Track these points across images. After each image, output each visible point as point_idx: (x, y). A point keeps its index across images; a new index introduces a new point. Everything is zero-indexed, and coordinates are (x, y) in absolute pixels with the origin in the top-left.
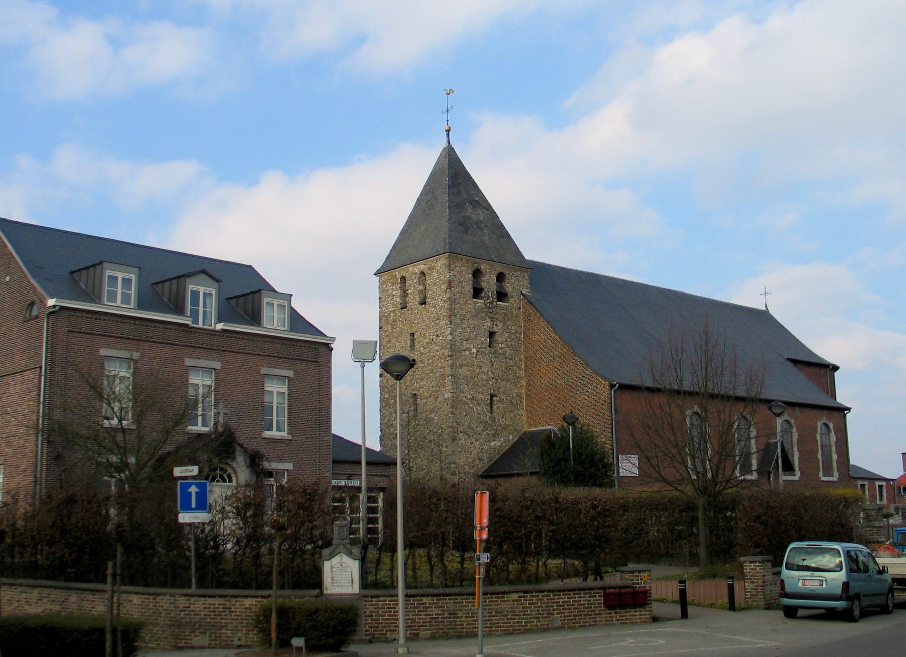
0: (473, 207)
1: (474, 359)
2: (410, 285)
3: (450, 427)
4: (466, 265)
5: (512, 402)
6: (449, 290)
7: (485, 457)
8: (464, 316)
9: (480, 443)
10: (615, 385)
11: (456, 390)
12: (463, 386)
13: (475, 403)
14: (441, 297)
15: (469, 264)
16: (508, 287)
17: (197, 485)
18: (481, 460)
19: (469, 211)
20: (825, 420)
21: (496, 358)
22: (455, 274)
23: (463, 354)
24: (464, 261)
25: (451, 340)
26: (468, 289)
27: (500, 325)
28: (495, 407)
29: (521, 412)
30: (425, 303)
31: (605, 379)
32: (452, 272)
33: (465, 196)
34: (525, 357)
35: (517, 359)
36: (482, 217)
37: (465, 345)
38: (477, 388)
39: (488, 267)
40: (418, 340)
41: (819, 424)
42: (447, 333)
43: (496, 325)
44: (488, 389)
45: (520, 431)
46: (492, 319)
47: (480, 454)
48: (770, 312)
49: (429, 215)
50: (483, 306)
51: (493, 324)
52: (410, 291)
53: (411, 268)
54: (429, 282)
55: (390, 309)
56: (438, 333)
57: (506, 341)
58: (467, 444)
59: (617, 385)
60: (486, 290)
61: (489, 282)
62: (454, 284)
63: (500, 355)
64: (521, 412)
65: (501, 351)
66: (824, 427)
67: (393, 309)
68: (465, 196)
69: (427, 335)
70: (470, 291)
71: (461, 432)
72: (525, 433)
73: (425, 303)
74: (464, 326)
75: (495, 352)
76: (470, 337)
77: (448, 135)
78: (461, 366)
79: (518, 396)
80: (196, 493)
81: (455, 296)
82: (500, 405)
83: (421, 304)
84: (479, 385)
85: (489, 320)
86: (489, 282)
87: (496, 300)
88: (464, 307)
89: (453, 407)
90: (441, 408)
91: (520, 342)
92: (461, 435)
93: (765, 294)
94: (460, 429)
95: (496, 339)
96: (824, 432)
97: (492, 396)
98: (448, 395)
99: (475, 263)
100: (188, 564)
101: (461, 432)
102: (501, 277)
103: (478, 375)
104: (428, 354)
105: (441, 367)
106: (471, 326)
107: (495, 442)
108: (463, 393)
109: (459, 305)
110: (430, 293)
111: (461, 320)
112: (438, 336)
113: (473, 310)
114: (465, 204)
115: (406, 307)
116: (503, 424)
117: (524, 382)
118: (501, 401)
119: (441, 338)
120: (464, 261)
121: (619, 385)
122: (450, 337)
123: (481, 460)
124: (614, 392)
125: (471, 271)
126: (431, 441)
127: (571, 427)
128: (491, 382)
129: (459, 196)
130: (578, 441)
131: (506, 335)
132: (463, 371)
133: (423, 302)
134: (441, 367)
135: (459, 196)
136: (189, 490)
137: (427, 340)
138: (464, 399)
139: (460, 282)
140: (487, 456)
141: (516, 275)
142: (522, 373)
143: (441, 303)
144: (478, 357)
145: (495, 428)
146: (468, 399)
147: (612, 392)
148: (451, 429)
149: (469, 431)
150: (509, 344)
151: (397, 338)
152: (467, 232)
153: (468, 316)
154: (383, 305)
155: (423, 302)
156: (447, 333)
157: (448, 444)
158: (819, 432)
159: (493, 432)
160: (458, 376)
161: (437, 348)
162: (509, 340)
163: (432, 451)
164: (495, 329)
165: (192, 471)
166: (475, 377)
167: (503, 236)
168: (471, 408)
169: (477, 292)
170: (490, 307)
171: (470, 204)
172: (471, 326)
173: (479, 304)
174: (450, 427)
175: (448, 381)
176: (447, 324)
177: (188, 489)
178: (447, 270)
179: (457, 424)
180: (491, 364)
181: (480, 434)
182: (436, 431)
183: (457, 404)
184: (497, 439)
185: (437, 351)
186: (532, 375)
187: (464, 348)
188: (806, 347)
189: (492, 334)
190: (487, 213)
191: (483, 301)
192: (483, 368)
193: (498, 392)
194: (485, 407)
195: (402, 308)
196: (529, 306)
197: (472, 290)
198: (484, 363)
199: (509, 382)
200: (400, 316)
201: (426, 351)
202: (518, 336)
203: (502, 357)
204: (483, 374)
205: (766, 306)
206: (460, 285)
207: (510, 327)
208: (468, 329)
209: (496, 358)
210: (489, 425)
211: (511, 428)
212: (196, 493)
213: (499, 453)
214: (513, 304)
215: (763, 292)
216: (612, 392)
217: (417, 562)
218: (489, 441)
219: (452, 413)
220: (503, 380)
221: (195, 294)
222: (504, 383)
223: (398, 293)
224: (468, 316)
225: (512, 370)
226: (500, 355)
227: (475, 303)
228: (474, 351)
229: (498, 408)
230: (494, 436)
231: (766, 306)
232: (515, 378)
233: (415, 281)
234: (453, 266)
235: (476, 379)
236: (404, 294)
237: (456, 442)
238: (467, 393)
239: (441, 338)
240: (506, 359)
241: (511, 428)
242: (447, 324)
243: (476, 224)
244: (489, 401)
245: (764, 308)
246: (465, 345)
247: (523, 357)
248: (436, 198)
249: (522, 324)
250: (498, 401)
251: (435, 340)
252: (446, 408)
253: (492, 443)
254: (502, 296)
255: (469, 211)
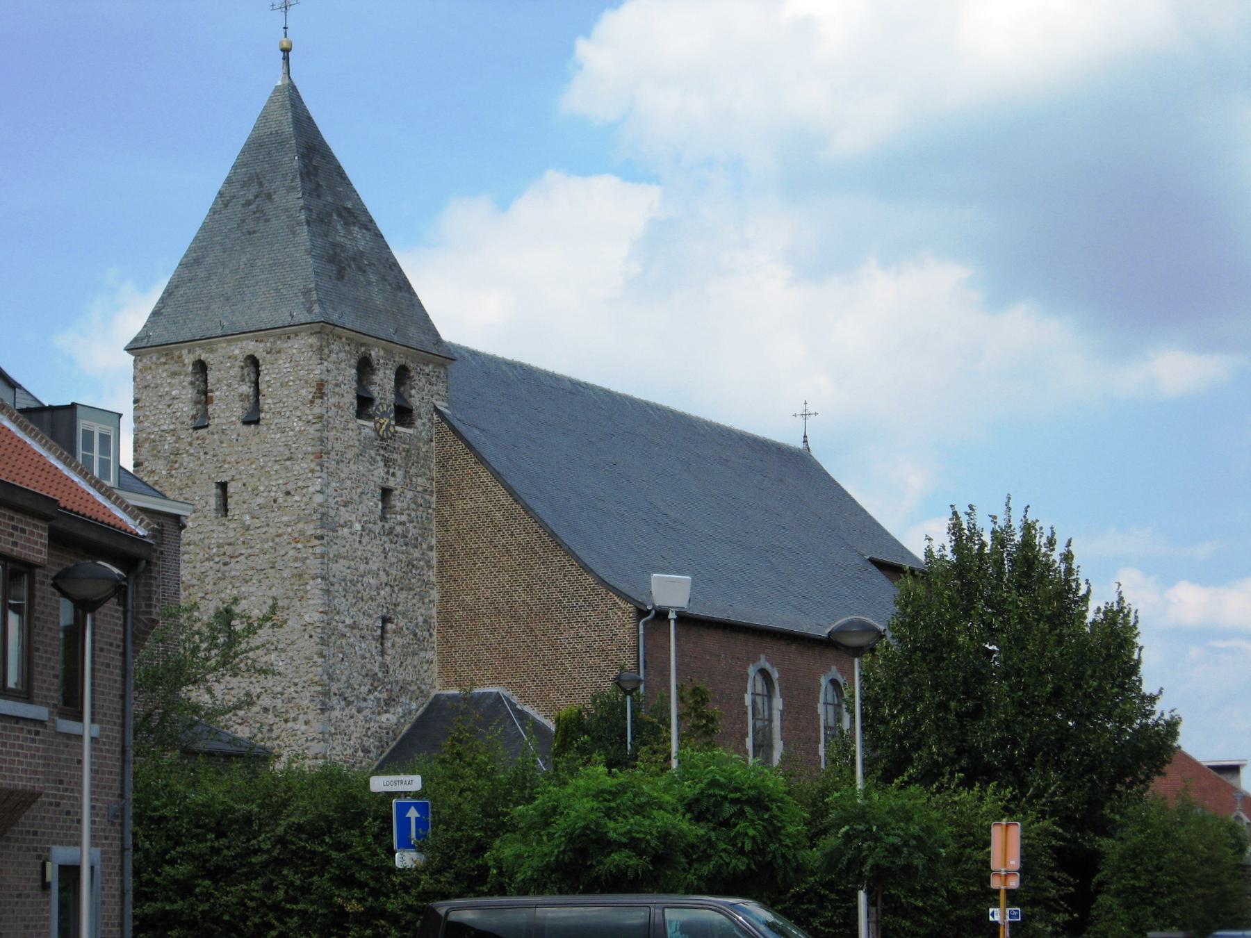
0: (346, 224)
1: (357, 545)
2: (219, 381)
3: (314, 683)
4: (347, 348)
5: (415, 635)
6: (318, 401)
7: (370, 743)
8: (343, 454)
9: (365, 717)
10: (649, 612)
11: (329, 610)
12: (341, 602)
13: (358, 636)
14: (299, 414)
15: (353, 347)
16: (416, 398)
17: (418, 806)
18: (366, 751)
19: (340, 234)
20: (764, 663)
21: (391, 542)
22: (331, 367)
23: (340, 533)
24: (344, 339)
25: (321, 505)
26: (350, 399)
27: (400, 474)
28: (388, 644)
29: (429, 655)
30: (257, 422)
31: (627, 598)
32: (326, 364)
33: (330, 199)
34: (439, 542)
35: (425, 546)
36: (362, 245)
37: (345, 514)
38: (362, 604)
39: (382, 353)
40: (236, 497)
41: (824, 681)
42: (311, 489)
43: (393, 475)
44: (378, 606)
45: (429, 693)
46: (387, 462)
47: (365, 739)
48: (816, 454)
49: (254, 232)
50: (372, 434)
51: (388, 473)
52: (217, 393)
53: (223, 348)
54: (267, 378)
55: (165, 427)
56: (290, 487)
57: (408, 508)
58: (344, 718)
59: (653, 612)
60: (377, 402)
61: (383, 384)
62: (328, 389)
63: (396, 536)
64: (429, 655)
65: (399, 529)
66: (830, 688)
67: (172, 427)
68: (330, 199)
69: (262, 489)
70: (352, 404)
71: (335, 694)
72: (437, 697)
73: (257, 422)
74: (343, 475)
75: (392, 529)
76: (351, 499)
77: (286, 59)
78: (337, 558)
79: (425, 621)
80: (416, 818)
81: (330, 414)
82: (397, 639)
83: (247, 423)
84: (365, 598)
85: (381, 464)
86: (383, 384)
87: (393, 422)
88: (342, 436)
89: (323, 642)
90: (293, 643)
91: (430, 511)
92: (335, 699)
93: (805, 415)
94: (334, 689)
95: (393, 503)
96: (830, 700)
97: (385, 620)
98: (312, 616)
99: (362, 345)
100: (472, 933)
101: (335, 694)
102: (402, 374)
103: (363, 576)
104: (264, 530)
105: (296, 560)
106: (354, 476)
107: (388, 715)
108: (338, 613)
109: (334, 432)
110: (270, 401)
111: (338, 463)
112: (288, 493)
113: (357, 444)
114: (331, 216)
115: (207, 426)
116: (400, 678)
117: (435, 594)
118: (398, 632)
119: (297, 498)
120: (344, 339)
121: (656, 612)
122: (319, 498)
123: (366, 751)
124: (645, 624)
125: (353, 362)
126: (266, 710)
127: (629, 698)
128: (382, 593)
129: (319, 197)
130: (1100, 756)
131: (409, 495)
132: (339, 568)
133: (252, 419)
134: (296, 560)
135: (319, 197)
136: (407, 816)
137: (260, 500)
138: (340, 625)
139: (337, 385)
140: (377, 743)
141: (427, 371)
142: (432, 576)
143: (298, 425)
144: (365, 540)
145: (389, 687)
146: (346, 627)
147: (641, 627)
148: (319, 688)
149: (348, 693)
150: (413, 514)
151: (180, 489)
152: (343, 277)
153: (349, 455)
154: (147, 417)
155: (252, 419)
156: (311, 489)
157: (310, 717)
158: (822, 700)
159: (385, 696)
160: (331, 579)
161: (285, 519)
162: (413, 506)
163: (271, 730)
164: (391, 484)
165: (410, 782)
166: (358, 582)
167: (400, 288)
168: (352, 646)
169: (364, 404)
170: (384, 440)
171: (340, 215)
172: (354, 476)
173: (367, 430)
174: (314, 683)
175: (314, 588)
176: (312, 471)
177: (406, 814)
178: (315, 359)
179: (331, 678)
180: (383, 555)
181: (365, 700)
182: (279, 689)
183: (329, 637)
184: (392, 710)
185: (287, 525)
186: (455, 581)
187: (342, 522)
188: (887, 534)
189: (386, 493)
190: (368, 235)
191: (371, 424)
192: (370, 562)
193: (395, 612)
194: (374, 644)
195: (196, 428)
196: (450, 437)
197: (355, 402)
198: (373, 554)
199: (412, 593)
200: (190, 444)
201: (257, 523)
202: (427, 497)
203: (401, 541)
204: (370, 576)
205: (805, 441)
206: (337, 390)
207: (414, 479)
208: (349, 482)
209: (391, 542)
210: (379, 680)
211: (414, 688)
212: (416, 818)
213: (395, 739)
214: (421, 432)
215: (800, 410)
216: (641, 627)
217: (1061, 914)
218: (379, 714)
219: (321, 655)
220: (402, 589)
221: (88, 435)
222: (403, 595)
223: (190, 393)
224: (349, 455)
225: (417, 568)
226: (396, 536)
227: (360, 427)
228: (357, 527)
229: (393, 645)
230: (389, 702)
231: (805, 441)
232: (422, 585)
233: (232, 373)
234: (326, 351)
235: (360, 584)
236: (204, 396)
237: (327, 714)
238: (346, 613)
239: (297, 498)
240: (407, 545)
241: (414, 688)
242: (312, 471)
243: (354, 259)
244: (379, 632)
245: (800, 445)
246: (345, 514)
247: (434, 542)
248: (269, 197)
249: (434, 474)
250: (394, 632)
251: (280, 500)
252: (309, 646)
253: (384, 717)
254: (403, 414)
255: (340, 234)
